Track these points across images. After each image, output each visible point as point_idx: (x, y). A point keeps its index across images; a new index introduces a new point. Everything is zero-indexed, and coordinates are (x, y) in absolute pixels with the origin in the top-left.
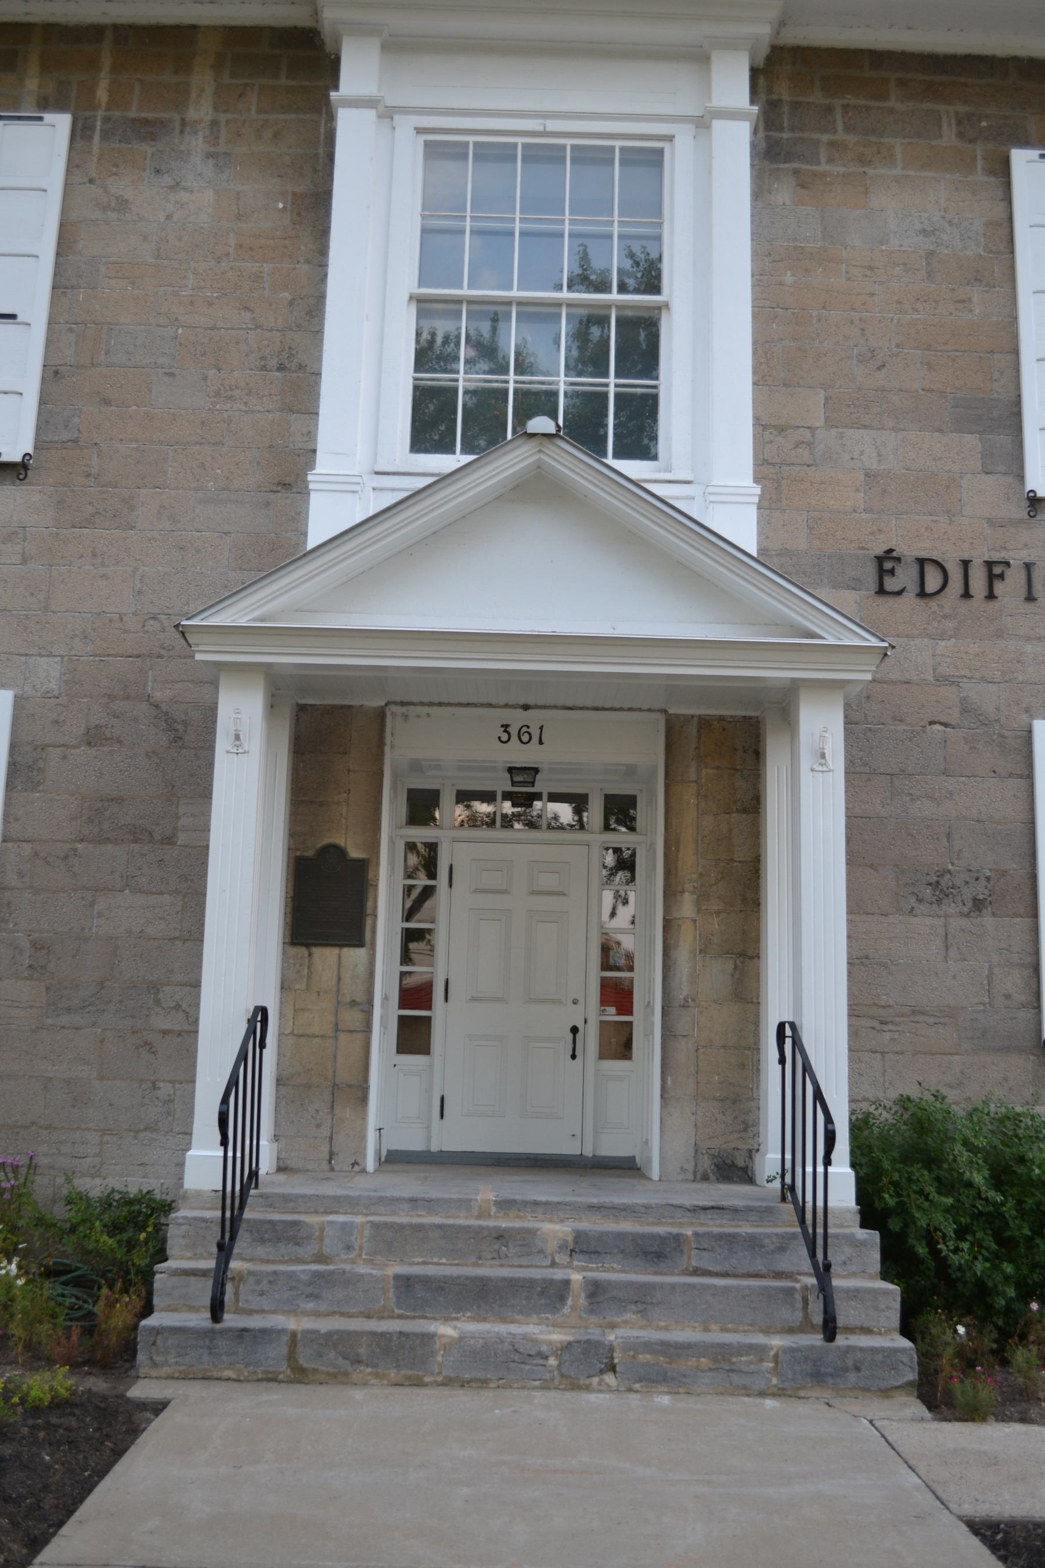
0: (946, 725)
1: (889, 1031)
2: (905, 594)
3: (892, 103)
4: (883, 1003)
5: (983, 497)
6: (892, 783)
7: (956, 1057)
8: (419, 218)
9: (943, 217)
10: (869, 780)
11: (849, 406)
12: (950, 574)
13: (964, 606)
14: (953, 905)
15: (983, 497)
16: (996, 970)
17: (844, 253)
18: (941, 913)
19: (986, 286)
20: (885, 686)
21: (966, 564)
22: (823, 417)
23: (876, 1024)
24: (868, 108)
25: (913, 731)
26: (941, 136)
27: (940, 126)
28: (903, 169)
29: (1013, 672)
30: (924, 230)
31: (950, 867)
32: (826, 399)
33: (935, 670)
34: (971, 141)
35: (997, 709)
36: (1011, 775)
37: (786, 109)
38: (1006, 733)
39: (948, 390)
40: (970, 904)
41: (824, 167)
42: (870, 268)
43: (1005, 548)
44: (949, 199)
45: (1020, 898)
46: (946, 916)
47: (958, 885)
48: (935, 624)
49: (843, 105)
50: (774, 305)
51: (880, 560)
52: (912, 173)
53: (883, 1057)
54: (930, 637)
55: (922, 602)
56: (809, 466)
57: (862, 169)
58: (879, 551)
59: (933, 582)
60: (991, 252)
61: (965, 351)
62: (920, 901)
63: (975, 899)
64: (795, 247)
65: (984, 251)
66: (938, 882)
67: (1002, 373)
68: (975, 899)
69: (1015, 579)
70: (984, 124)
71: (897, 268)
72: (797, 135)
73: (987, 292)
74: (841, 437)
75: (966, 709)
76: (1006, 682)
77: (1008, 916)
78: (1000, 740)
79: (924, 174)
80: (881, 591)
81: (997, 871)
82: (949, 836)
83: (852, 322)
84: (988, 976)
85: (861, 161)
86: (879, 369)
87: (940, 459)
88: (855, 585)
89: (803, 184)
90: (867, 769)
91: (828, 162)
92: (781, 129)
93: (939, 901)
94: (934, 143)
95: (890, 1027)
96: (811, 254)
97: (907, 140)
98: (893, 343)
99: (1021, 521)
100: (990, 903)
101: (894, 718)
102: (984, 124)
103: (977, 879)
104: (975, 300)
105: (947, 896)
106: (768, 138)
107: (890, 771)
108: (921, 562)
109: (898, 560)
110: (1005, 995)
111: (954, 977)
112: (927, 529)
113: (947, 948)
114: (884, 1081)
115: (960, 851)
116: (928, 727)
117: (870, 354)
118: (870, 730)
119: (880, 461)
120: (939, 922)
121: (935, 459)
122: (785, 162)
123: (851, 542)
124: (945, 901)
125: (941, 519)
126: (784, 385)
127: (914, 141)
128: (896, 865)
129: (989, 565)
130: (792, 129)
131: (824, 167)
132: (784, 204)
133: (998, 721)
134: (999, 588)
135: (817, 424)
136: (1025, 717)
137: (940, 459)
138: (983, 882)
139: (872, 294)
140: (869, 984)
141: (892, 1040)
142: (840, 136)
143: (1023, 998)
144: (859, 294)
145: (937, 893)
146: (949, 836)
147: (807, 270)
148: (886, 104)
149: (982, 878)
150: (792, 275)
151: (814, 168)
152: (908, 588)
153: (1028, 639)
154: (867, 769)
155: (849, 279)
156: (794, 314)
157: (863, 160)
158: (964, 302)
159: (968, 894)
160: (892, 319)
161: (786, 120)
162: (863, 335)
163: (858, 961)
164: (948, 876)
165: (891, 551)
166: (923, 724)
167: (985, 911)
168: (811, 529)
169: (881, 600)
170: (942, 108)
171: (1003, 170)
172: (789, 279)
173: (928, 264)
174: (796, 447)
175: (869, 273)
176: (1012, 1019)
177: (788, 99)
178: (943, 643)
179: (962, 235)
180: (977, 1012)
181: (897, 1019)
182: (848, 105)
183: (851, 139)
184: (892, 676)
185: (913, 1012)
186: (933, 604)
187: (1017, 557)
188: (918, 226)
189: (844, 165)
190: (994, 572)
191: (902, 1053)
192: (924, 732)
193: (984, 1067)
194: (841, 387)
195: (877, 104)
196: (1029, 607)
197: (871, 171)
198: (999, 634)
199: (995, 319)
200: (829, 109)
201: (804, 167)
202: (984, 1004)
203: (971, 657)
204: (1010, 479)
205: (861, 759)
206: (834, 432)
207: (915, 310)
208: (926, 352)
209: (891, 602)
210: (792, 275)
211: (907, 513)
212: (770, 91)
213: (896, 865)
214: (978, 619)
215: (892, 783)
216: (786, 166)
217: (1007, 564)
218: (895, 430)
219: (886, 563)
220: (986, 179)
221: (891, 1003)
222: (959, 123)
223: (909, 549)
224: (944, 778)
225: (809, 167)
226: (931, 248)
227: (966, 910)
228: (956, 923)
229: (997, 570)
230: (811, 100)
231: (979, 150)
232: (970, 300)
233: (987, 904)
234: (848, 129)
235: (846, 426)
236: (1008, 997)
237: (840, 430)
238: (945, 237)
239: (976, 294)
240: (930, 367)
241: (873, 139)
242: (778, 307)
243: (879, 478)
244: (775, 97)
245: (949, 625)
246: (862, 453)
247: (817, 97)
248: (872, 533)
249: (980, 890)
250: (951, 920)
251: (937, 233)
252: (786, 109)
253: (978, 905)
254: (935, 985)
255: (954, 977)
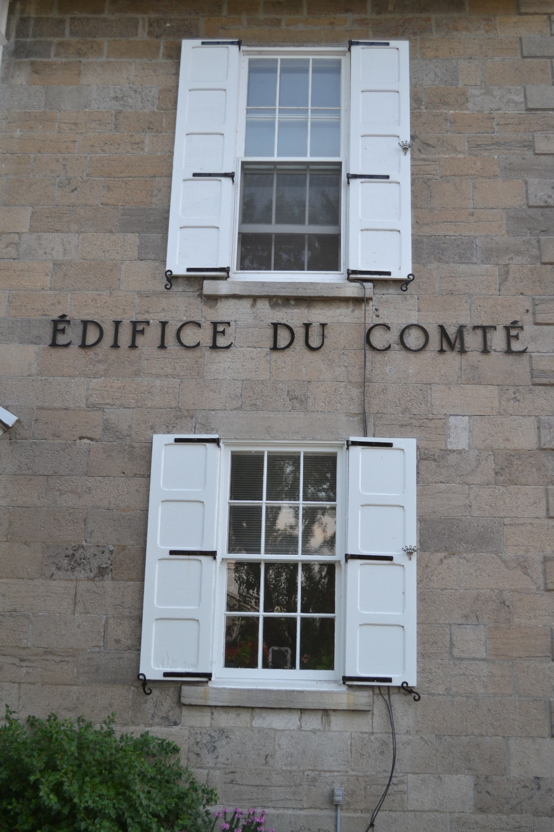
0: (91, 439)
1: (26, 666)
2: (71, 346)
3: (106, 15)
4: (23, 645)
5: (137, 277)
6: (47, 482)
7: (75, 687)
8: (245, 111)
9: (131, 88)
10: (31, 480)
11: (47, 217)
12: (105, 331)
13: (114, 354)
14: (83, 572)
15: (137, 277)
16: (111, 621)
17: (58, 115)
18: (73, 577)
19: (155, 132)
20: (50, 412)
21: (117, 324)
22: (28, 226)
23: (16, 661)
24: (88, 19)
25: (66, 444)
26: (137, 35)
27: (137, 28)
28: (108, 57)
29: (144, 400)
30: (117, 97)
31: (84, 543)
32: (33, 213)
33: (87, 400)
34: (157, 37)
35: (130, 427)
36: (135, 475)
37: (32, 22)
38: (135, 444)
39: (120, 204)
40: (95, 571)
41: (53, 59)
42: (75, 124)
43: (148, 312)
44: (137, 76)
45: (134, 566)
46: (77, 580)
47: (88, 557)
48: (91, 367)
49: (71, 18)
50: (5, 152)
51: (55, 323)
52: (113, 60)
53: (20, 687)
54: (86, 376)
55: (83, 352)
56: (14, 259)
57: (78, 59)
58: (56, 317)
59: (92, 337)
60: (162, 109)
61: (135, 177)
62: (59, 569)
63: (99, 567)
64: (25, 113)
65: (157, 109)
66: (73, 555)
67: (159, 191)
68: (99, 567)
69: (153, 334)
70: (168, 25)
71: (94, 123)
72: (37, 39)
73: (155, 136)
74: (39, 238)
75: (107, 428)
76: (138, 407)
77: (123, 580)
78: (130, 449)
79: (120, 60)
80: (54, 345)
81: (119, 546)
82: (85, 521)
83: (58, 161)
84: (104, 626)
85: (79, 54)
86: (72, 191)
87: (108, 251)
88: (36, 341)
89: (36, 69)
90: (30, 472)
91: (55, 56)
92: (27, 36)
93: (73, 569)
94: (131, 39)
95: (27, 664)
96: (36, 116)
97: (113, 38)
98: (85, 174)
99: (162, 293)
100: (111, 570)
101: (54, 435)
102: (168, 25)
103: (103, 552)
104: (147, 142)
105: (79, 565)
106: (17, 42)
107: (46, 473)
108: (85, 323)
109: (68, 322)
110: (115, 640)
111: (79, 626)
112: (93, 300)
113: (75, 604)
114: (19, 705)
115: (92, 531)
116: (78, 441)
117: (67, 182)
118: (35, 443)
119: (64, 254)
120: (71, 585)
121: (104, 252)
122: (26, 57)
123: (38, 310)
124: (78, 569)
125: (104, 293)
126: (5, 205)
127: (117, 39)
128: (44, 542)
129: (134, 324)
130: (34, 36)
131: (53, 59)
132: (21, 85)
133: (129, 435)
134: (140, 340)
135: (24, 231)
136: (150, 432)
137: (108, 251)
138: (107, 555)
139: (74, 142)
140: (15, 631)
141: (28, 673)
142: (67, 38)
143: (129, 642)
144: (65, 142)
145: (72, 563)
146: (85, 521)
147: (31, 128)
148: (102, 16)
149: (107, 551)
150: (21, 131)
151: (46, 60)
152: (73, 341)
153: (158, 376)
154: (30, 472)
155: (59, 132)
156: (18, 157)
157: (79, 53)
158: (139, 144)
159: (95, 563)
160: (86, 157)
161: (31, 30)
162: (64, 169)
163: (8, 614)
164: (82, 550)
165: (64, 316)
166: (74, 438)
167: (106, 576)
168: (10, 302)
169: (53, 351)
170: (139, 16)
171: (175, 54)
172: (18, 133)
173: (116, 119)
174: (7, 246)
175: (74, 127)
176: (119, 658)
177: (34, 16)
178: (96, 380)
179: (142, 99)
180: (93, 653)
181: (33, 658)
182: (75, 18)
183: (74, 40)
184: (56, 405)
185: (45, 652)
186: (91, 353)
187: (154, 319)
188: (112, 94)
189: (66, 57)
190: (138, 329)
191: (34, 684)
192: (74, 444)
193: (95, 696)
194: (44, 205)
195: (95, 16)
196: (162, 352)
197: (83, 60)
198: (137, 373)
199: (159, 154)
200: (62, 21)
201: (38, 59)
202: (99, 647)
203: (115, 390)
204: (157, 264)
205: (27, 464)
206: (35, 235)
207: (103, 151)
208: (108, 179)
209: (61, 352)
210: (21, 131)
211: (80, 289)
212: (23, 11)
213: (44, 542)
214: (123, 363)
215: (47, 482)
216: (27, 60)
217: (148, 323)
218: (78, 232)
219: (60, 324)
220: (164, 61)
221: (29, 644)
222: (150, 25)
223: (76, 314)
224: (86, 478)
225: (42, 60)
226: (120, 108)
227: (92, 575)
228: (84, 585)
229: (220, 328)
230: (50, 16)
231: (162, 43)
232: (143, 142)
233: (109, 571)
234: (72, 33)
235: (44, 232)
236: (118, 641)
237: (40, 234)
238: (130, 101)
239: (148, 138)
240: (109, 189)
241: (89, 39)
242: (8, 153)
243: (63, 266)
244: (25, 15)
245: (101, 367)
246: (53, 249)
247: (55, 14)
248: (53, 304)
249: (104, 560)
250: (81, 582)
251: (125, 98)
252: (32, 22)
253: (102, 572)
254: (63, 632)
255: (79, 626)
